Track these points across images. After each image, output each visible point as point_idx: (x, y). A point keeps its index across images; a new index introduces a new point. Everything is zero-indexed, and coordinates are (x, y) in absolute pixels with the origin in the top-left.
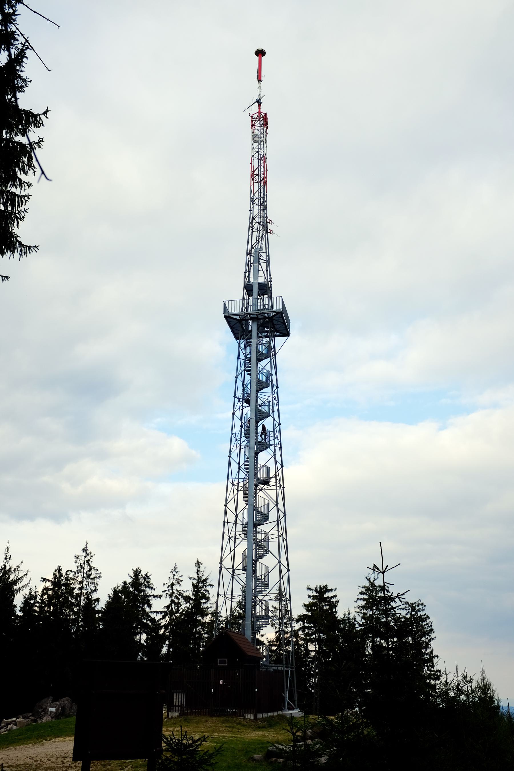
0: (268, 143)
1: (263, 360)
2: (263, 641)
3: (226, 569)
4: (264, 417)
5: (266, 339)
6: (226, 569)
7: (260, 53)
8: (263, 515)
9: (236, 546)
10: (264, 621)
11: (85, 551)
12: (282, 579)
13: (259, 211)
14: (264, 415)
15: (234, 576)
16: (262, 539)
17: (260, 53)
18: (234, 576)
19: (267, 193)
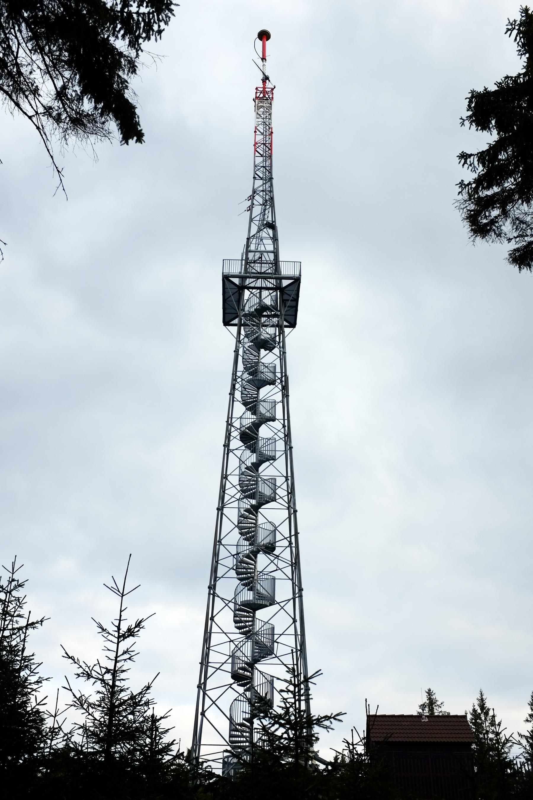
0: (290, 398)
1: (270, 502)
2: (486, 89)
3: (238, 401)
4: (260, 657)
5: (172, 755)
6: (238, 401)
7: (264, 36)
8: (259, 594)
9: (208, 677)
10: (242, 744)
11: (264, 92)
12: (202, 681)
13: (257, 245)
14: (264, 651)
15: (207, 692)
16: (246, 643)
17: (264, 36)
18: (207, 692)
19: (367, 709)
